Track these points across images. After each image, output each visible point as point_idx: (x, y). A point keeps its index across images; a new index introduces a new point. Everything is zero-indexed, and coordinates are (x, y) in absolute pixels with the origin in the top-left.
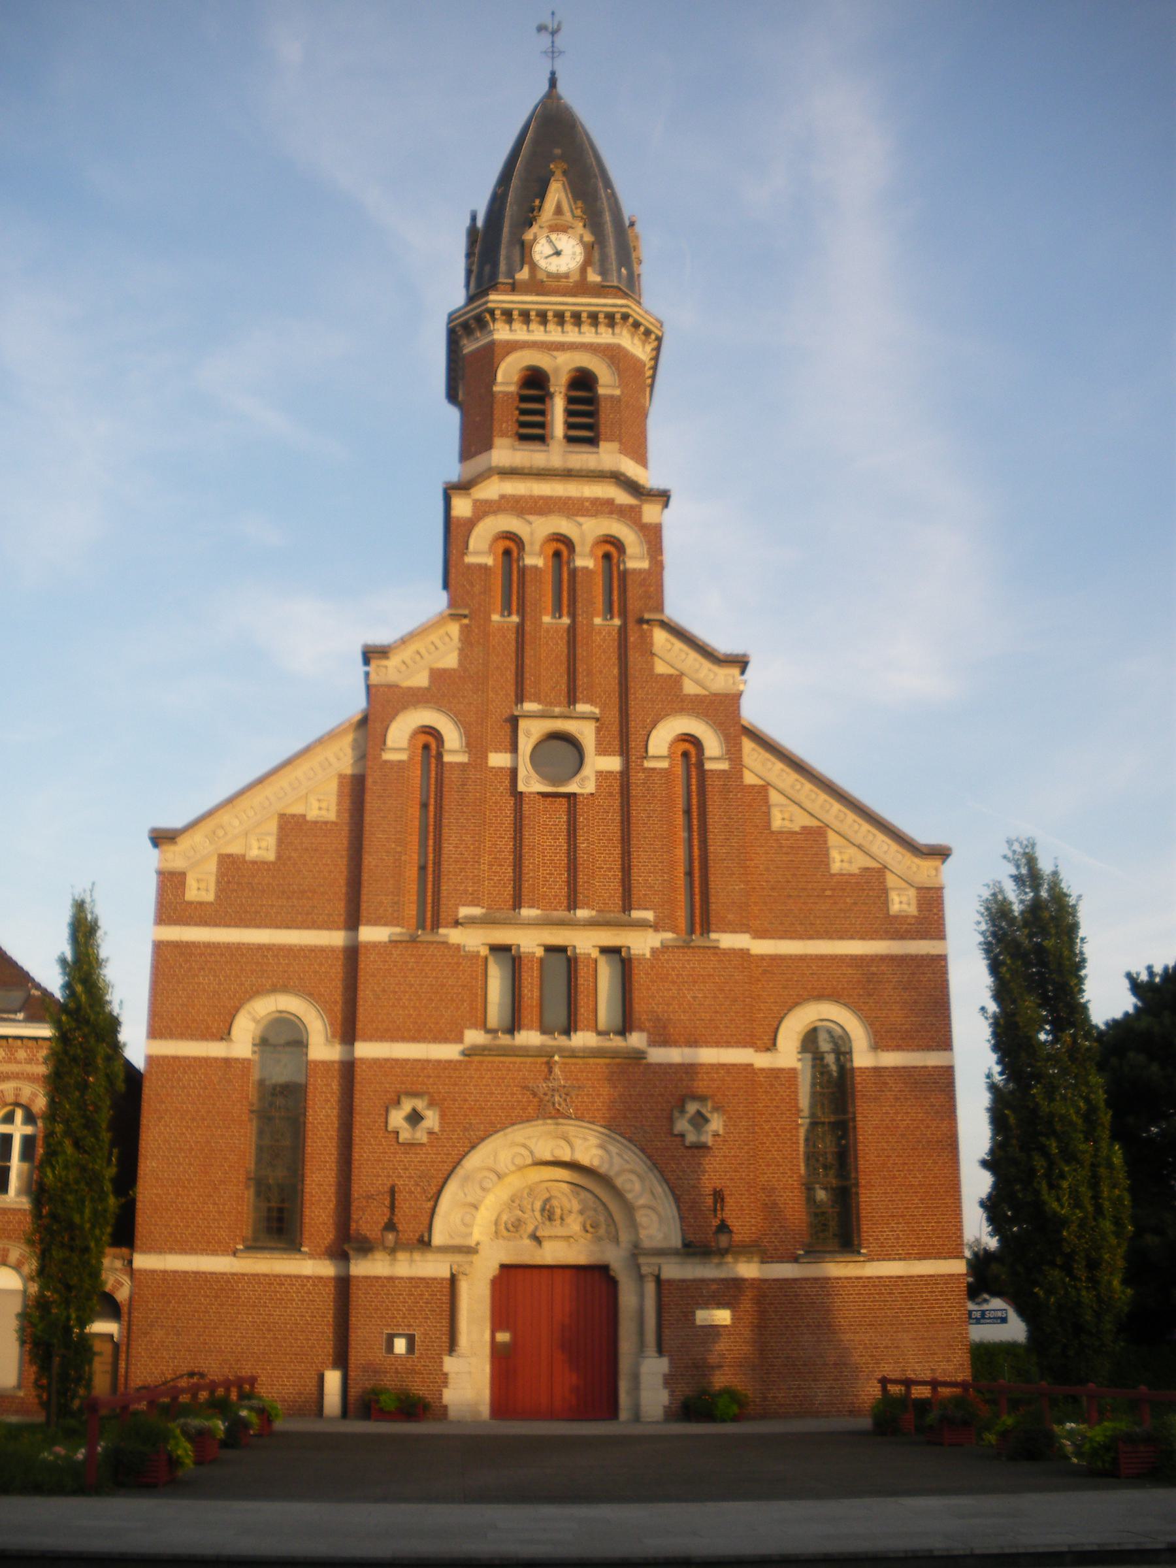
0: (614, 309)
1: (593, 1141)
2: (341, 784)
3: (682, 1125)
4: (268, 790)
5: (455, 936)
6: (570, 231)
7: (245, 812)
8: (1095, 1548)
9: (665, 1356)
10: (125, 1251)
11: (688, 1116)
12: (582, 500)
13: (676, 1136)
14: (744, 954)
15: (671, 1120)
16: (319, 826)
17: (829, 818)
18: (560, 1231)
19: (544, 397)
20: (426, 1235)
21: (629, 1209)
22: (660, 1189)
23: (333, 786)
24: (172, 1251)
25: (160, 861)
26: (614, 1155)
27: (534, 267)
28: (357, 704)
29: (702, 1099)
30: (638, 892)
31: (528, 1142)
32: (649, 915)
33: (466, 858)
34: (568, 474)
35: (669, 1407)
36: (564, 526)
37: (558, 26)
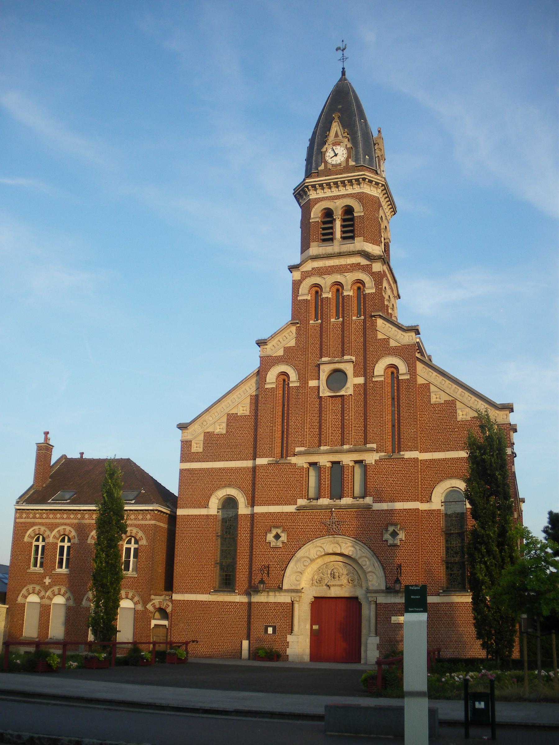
0: (359, 177)
1: (349, 544)
2: (251, 399)
3: (387, 536)
4: (223, 404)
5: (293, 460)
6: (341, 144)
7: (214, 414)
8: (209, 708)
9: (378, 636)
10: (170, 592)
11: (389, 532)
12: (346, 265)
13: (384, 541)
14: (416, 460)
15: (382, 534)
16: (244, 417)
17: (457, 396)
18: (337, 582)
19: (332, 221)
20: (281, 585)
21: (365, 573)
22: (377, 564)
23: (248, 400)
24: (186, 593)
25: (182, 437)
26: (358, 550)
27: (326, 163)
28: (256, 365)
29: (395, 525)
30: (370, 436)
31: (322, 545)
32: (374, 446)
33: (299, 427)
34: (340, 255)
35: (379, 658)
36: (338, 278)
37: (345, 46)
